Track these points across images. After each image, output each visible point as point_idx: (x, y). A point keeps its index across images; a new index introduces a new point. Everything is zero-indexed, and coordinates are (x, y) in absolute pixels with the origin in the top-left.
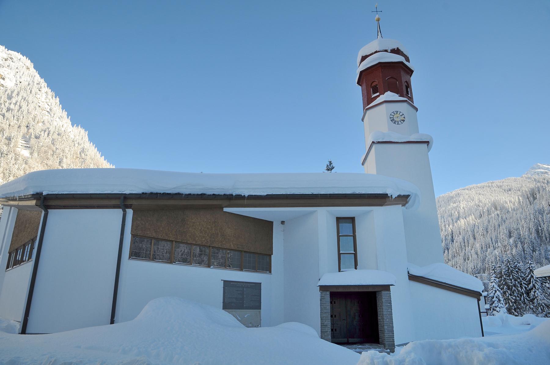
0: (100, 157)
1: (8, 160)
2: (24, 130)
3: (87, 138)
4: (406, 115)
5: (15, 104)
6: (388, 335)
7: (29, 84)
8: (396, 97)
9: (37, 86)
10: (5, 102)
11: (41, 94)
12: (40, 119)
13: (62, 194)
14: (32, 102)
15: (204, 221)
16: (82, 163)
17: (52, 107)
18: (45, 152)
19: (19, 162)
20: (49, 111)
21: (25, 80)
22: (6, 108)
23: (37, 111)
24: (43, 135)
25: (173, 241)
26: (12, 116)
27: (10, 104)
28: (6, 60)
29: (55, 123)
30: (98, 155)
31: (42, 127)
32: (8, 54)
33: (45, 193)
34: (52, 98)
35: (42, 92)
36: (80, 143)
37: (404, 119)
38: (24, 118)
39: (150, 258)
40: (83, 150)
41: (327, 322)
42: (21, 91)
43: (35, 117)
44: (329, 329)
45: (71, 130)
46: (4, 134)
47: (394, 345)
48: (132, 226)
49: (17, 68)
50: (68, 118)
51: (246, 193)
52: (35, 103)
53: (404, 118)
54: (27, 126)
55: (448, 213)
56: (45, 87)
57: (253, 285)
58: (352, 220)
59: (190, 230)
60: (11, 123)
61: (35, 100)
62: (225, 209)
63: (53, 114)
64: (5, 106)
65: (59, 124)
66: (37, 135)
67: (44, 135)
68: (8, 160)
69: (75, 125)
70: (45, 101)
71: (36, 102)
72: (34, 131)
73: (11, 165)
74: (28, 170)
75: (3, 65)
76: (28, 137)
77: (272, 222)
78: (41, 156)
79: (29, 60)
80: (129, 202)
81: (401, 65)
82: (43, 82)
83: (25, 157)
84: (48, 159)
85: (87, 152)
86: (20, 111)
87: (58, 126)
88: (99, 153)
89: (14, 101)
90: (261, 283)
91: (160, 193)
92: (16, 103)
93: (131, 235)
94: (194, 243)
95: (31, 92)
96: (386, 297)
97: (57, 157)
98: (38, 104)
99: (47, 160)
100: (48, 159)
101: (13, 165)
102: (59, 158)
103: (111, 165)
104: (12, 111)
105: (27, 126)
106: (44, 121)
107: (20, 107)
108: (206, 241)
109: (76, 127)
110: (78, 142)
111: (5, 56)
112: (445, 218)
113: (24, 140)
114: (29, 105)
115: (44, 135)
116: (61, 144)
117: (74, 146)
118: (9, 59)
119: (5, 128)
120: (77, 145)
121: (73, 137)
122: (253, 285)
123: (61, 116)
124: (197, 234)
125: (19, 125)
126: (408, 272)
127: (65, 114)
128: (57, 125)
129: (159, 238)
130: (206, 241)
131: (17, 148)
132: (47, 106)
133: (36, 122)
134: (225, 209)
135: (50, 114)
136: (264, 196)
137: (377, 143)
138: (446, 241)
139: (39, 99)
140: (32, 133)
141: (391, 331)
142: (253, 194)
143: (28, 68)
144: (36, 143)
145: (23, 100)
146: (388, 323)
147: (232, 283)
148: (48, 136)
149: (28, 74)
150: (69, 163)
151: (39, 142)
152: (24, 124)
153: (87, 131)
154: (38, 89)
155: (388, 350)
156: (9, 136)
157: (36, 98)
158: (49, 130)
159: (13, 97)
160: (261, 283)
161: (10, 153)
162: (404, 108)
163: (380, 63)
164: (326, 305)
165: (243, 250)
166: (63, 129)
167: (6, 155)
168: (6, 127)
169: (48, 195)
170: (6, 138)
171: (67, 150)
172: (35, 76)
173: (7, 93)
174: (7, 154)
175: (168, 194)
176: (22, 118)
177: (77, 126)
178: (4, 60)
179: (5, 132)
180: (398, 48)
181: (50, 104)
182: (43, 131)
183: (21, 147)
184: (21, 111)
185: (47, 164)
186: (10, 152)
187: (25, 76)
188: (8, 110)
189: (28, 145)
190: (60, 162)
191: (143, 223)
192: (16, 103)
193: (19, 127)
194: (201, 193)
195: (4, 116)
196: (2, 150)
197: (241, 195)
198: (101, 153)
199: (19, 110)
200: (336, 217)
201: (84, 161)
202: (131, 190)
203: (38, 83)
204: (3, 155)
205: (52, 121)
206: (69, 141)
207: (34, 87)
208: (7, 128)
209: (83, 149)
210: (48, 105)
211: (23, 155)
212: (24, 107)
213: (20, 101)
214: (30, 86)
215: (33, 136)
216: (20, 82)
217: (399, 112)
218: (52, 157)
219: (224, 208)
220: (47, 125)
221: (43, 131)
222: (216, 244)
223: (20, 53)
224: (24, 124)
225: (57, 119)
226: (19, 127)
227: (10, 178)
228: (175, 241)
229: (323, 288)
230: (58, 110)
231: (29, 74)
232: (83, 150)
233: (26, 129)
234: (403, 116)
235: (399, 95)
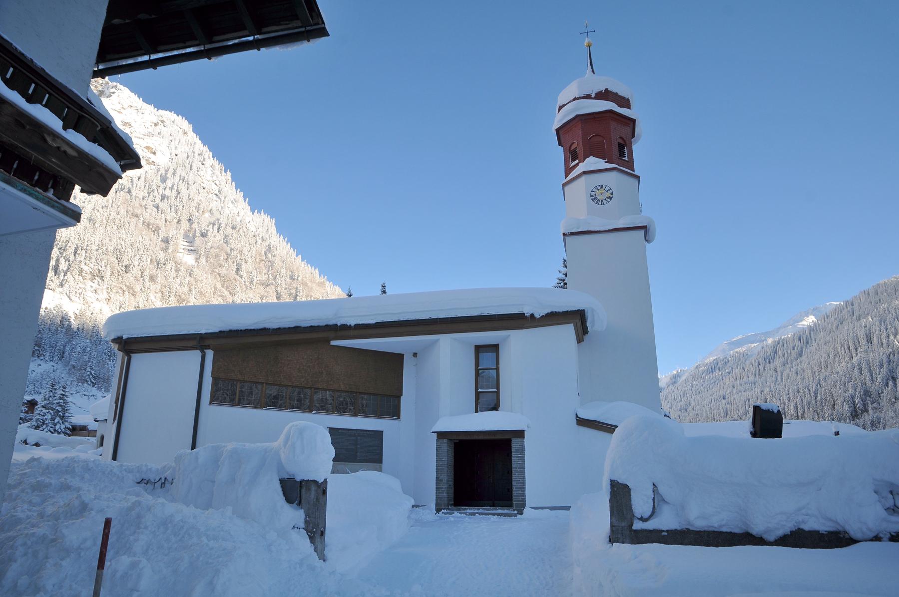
0: (295, 257)
1: (167, 273)
2: (185, 225)
3: (274, 229)
4: (614, 190)
5: (172, 188)
6: (517, 492)
7: (188, 157)
8: (601, 164)
9: (199, 158)
10: (158, 187)
11: (205, 169)
12: (206, 207)
13: (141, 337)
14: (194, 183)
15: (303, 358)
16: (269, 268)
17: (221, 187)
18: (216, 256)
19: (181, 274)
20: (218, 193)
21: (183, 151)
22: (160, 195)
23: (200, 195)
24: (211, 230)
25: (263, 383)
26: (169, 206)
27: (165, 190)
28: (156, 125)
29: (227, 211)
30: (293, 254)
31: (209, 218)
32: (158, 116)
33: (125, 337)
34: (221, 173)
35: (206, 166)
36: (264, 238)
37: (611, 196)
38: (185, 207)
39: (235, 403)
40: (269, 249)
41: (442, 477)
42: (178, 167)
43: (199, 205)
44: (444, 485)
45: (250, 219)
46: (160, 234)
47: (524, 506)
48: (213, 368)
49: (171, 135)
50: (245, 201)
51: (352, 322)
52: (197, 183)
53: (612, 194)
54: (190, 220)
55: (894, 314)
56: (209, 158)
57: (372, 433)
58: (495, 348)
59: (285, 369)
60: (168, 218)
61: (198, 179)
62: (333, 343)
63: (223, 197)
64: (159, 193)
65: (232, 212)
66: (204, 231)
67: (213, 231)
68: (167, 273)
69: (256, 211)
70: (211, 179)
71: (199, 182)
72: (200, 225)
73: (171, 279)
74: (194, 286)
75: (153, 133)
76: (191, 236)
77: (402, 355)
78: (211, 263)
79: (186, 120)
80: (207, 342)
82: (206, 151)
83: (189, 265)
84: (220, 266)
85: (275, 251)
86: (179, 197)
87: (232, 214)
88: (294, 251)
89: (169, 183)
90: (383, 431)
91: (241, 330)
92: (173, 186)
93: (211, 378)
94: (290, 384)
95: (191, 169)
96: (517, 445)
97: (233, 263)
98: (202, 184)
99: (219, 268)
100: (220, 266)
101: (174, 278)
102: (235, 264)
103: (313, 268)
104: (168, 200)
105: (190, 220)
106: (211, 210)
107: (179, 193)
108: (305, 382)
109: (257, 213)
110: (261, 236)
111: (155, 120)
112: (888, 322)
113: (186, 240)
114: (190, 188)
115: (213, 231)
116: (237, 242)
117: (256, 243)
118: (160, 123)
119: (160, 226)
120: (259, 241)
121: (254, 229)
122: (372, 433)
123: (235, 200)
124: (294, 374)
125: (178, 218)
126: (577, 415)
127: (240, 195)
128: (230, 213)
129: (245, 380)
130: (305, 382)
131: (178, 253)
132: (214, 186)
133: (201, 212)
134: (333, 343)
135: (219, 198)
136: (373, 324)
137: (570, 235)
138: (890, 364)
139: (202, 177)
140: (197, 229)
141: (521, 488)
142: (361, 323)
143: (185, 133)
144: (203, 244)
145: (181, 181)
146: (517, 478)
147: (350, 432)
148: (218, 232)
149: (186, 142)
150: (250, 270)
151: (206, 242)
152: (185, 217)
153: (274, 219)
154: (200, 163)
155: (516, 512)
156: (166, 236)
157: (198, 176)
158: (220, 222)
159: (167, 178)
160: (383, 431)
161: (169, 261)
162: (614, 180)
163: (577, 116)
164: (442, 456)
165: (358, 391)
166: (239, 219)
167: (164, 265)
168: (161, 224)
169: (128, 338)
170: (162, 240)
171: (246, 250)
172: (195, 143)
173: (160, 173)
174: (165, 263)
175: (251, 330)
176: (181, 207)
177: (259, 212)
178: (153, 125)
179: (160, 231)
180: (606, 90)
181: (218, 183)
182: (211, 225)
183: (182, 251)
184: (180, 198)
185: (219, 274)
186: (169, 259)
187: (182, 145)
188: (163, 198)
189: (192, 248)
190: (238, 270)
191: (226, 364)
192: (173, 186)
193: (179, 222)
194: (278, 327)
195: (157, 207)
196: (159, 259)
197: (347, 325)
198: (296, 250)
199: (177, 197)
200: (475, 346)
201: (272, 266)
202: (207, 330)
203: (199, 153)
204: (159, 266)
205: (222, 208)
206: (248, 236)
207: (195, 159)
208: (164, 225)
209: (269, 246)
210: (216, 184)
211: (186, 263)
212: (184, 193)
213: (178, 183)
214: (189, 158)
215: (198, 234)
216: (176, 155)
217: (604, 187)
218: (226, 262)
219: (331, 341)
220: (217, 215)
221: (211, 225)
222: (320, 385)
223: (173, 112)
224: (185, 216)
225: (230, 205)
226: (179, 222)
227: (170, 299)
228: (266, 383)
229: (441, 435)
230: (230, 191)
231: (187, 141)
232: (269, 249)
233: (188, 224)
234: (611, 191)
235: (606, 160)
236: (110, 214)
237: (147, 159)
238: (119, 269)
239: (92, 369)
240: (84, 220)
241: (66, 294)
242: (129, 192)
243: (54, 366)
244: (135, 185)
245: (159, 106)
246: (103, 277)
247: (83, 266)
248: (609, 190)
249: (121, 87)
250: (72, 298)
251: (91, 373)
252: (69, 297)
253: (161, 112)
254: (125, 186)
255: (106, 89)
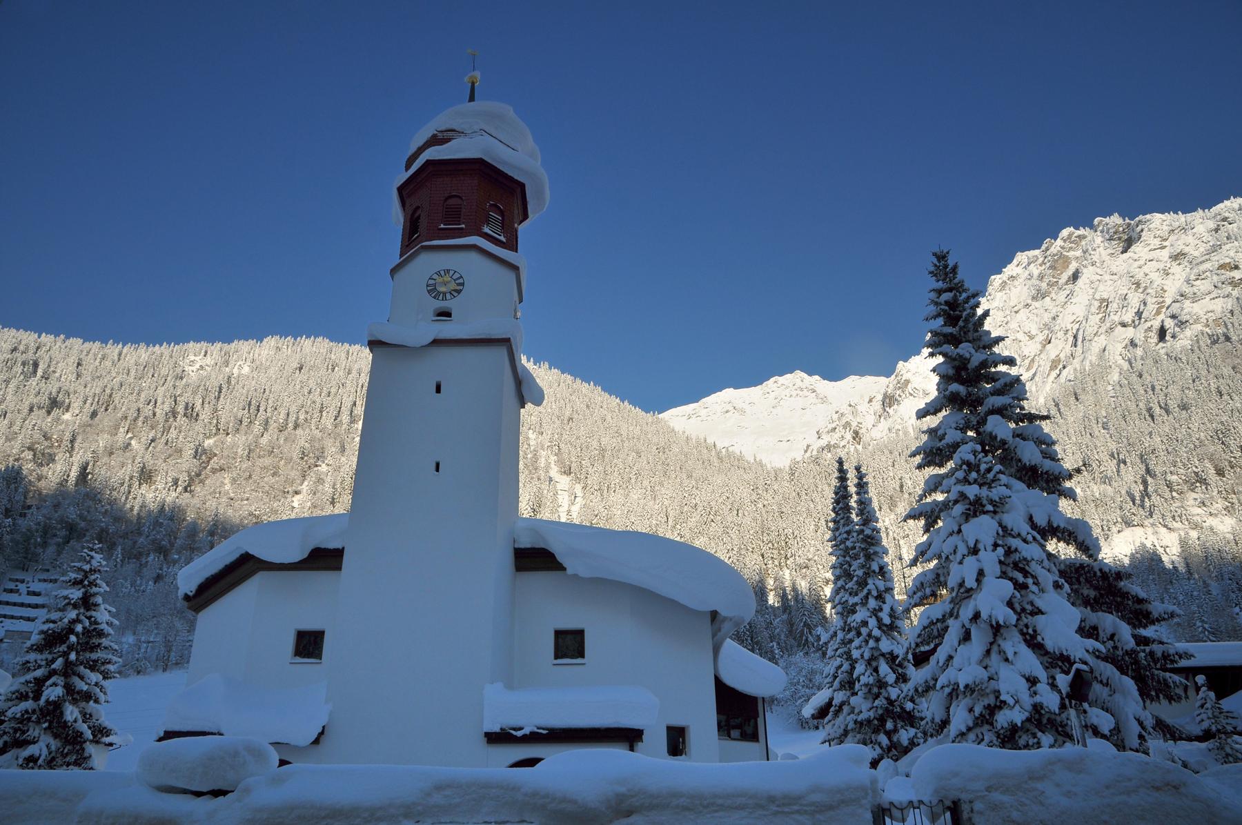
28: (1217, 230)
32: (1214, 217)
75: (1219, 243)
81: (519, 190)
217: (451, 273)
236: (1209, 384)
237: (1230, 281)
238: (1227, 457)
239: (1203, 621)
240: (1175, 410)
241: (1160, 523)
242: (1228, 339)
243: (1157, 631)
244: (1230, 326)
245: (1208, 204)
246: (1205, 479)
247: (1169, 477)
248: (458, 278)
249: (1148, 216)
250: (1170, 525)
251: (1204, 628)
252: (1165, 526)
253: (1215, 209)
254: (1217, 335)
255: (1132, 233)
